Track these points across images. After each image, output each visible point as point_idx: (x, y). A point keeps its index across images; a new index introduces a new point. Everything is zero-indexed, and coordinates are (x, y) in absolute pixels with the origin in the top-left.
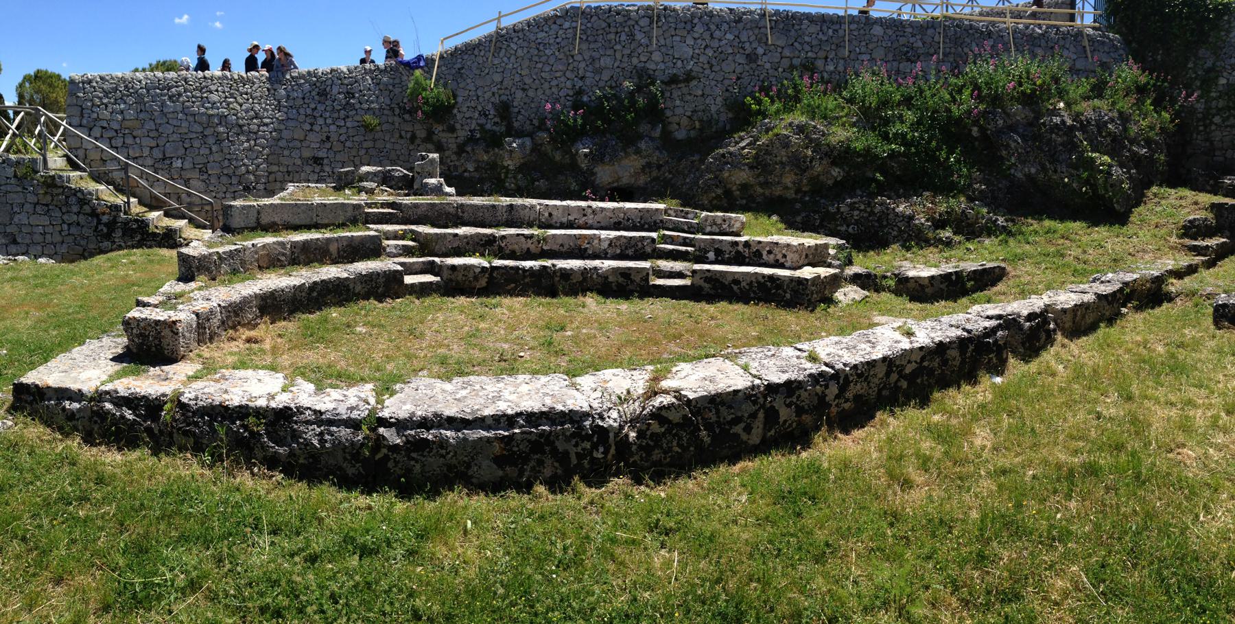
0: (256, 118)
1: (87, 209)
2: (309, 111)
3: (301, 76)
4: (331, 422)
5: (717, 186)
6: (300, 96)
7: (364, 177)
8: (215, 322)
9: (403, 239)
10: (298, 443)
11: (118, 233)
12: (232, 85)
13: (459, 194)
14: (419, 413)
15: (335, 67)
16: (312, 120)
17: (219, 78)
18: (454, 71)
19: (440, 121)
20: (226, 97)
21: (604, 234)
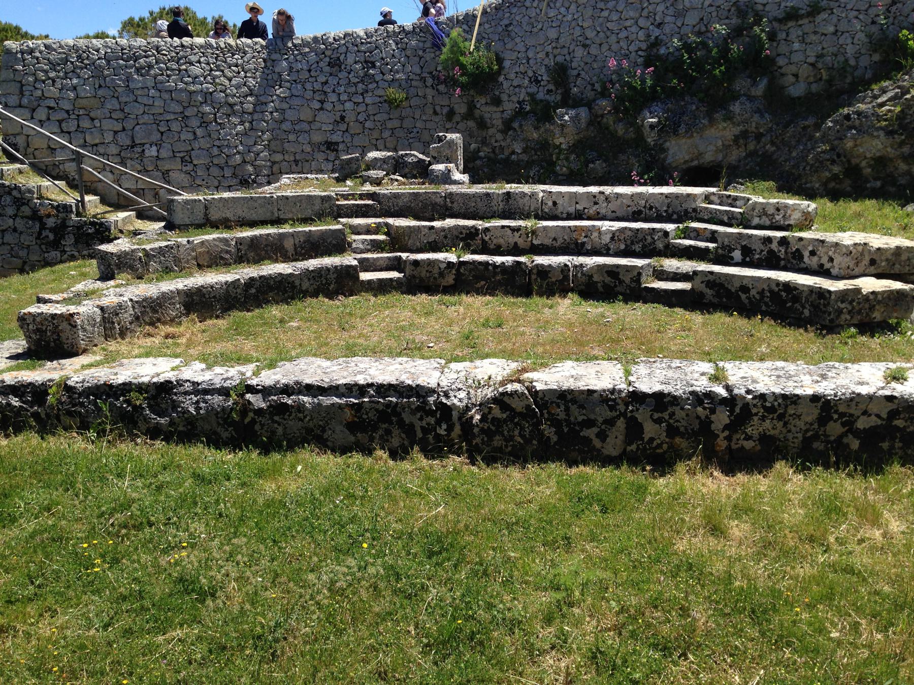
0: (251, 95)
1: (26, 210)
2: (317, 86)
3: (305, 43)
4: (206, 392)
5: (833, 162)
6: (305, 68)
7: (373, 164)
8: (127, 317)
9: (377, 234)
10: (177, 412)
11: (69, 241)
12: (218, 55)
13: (474, 181)
14: (283, 381)
15: (349, 30)
16: (323, 97)
17: (202, 46)
18: (500, 29)
19: (482, 92)
20: (211, 70)
21: (606, 225)
